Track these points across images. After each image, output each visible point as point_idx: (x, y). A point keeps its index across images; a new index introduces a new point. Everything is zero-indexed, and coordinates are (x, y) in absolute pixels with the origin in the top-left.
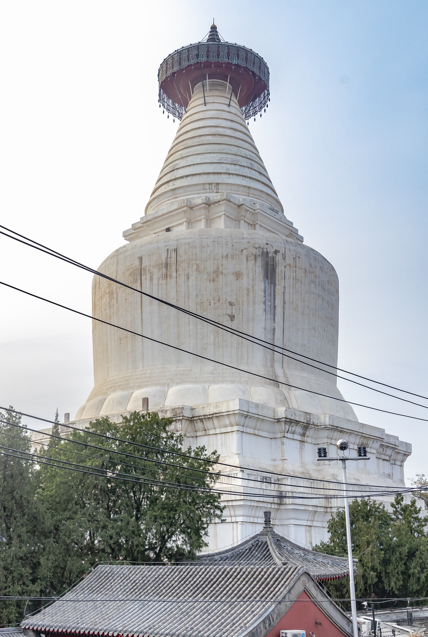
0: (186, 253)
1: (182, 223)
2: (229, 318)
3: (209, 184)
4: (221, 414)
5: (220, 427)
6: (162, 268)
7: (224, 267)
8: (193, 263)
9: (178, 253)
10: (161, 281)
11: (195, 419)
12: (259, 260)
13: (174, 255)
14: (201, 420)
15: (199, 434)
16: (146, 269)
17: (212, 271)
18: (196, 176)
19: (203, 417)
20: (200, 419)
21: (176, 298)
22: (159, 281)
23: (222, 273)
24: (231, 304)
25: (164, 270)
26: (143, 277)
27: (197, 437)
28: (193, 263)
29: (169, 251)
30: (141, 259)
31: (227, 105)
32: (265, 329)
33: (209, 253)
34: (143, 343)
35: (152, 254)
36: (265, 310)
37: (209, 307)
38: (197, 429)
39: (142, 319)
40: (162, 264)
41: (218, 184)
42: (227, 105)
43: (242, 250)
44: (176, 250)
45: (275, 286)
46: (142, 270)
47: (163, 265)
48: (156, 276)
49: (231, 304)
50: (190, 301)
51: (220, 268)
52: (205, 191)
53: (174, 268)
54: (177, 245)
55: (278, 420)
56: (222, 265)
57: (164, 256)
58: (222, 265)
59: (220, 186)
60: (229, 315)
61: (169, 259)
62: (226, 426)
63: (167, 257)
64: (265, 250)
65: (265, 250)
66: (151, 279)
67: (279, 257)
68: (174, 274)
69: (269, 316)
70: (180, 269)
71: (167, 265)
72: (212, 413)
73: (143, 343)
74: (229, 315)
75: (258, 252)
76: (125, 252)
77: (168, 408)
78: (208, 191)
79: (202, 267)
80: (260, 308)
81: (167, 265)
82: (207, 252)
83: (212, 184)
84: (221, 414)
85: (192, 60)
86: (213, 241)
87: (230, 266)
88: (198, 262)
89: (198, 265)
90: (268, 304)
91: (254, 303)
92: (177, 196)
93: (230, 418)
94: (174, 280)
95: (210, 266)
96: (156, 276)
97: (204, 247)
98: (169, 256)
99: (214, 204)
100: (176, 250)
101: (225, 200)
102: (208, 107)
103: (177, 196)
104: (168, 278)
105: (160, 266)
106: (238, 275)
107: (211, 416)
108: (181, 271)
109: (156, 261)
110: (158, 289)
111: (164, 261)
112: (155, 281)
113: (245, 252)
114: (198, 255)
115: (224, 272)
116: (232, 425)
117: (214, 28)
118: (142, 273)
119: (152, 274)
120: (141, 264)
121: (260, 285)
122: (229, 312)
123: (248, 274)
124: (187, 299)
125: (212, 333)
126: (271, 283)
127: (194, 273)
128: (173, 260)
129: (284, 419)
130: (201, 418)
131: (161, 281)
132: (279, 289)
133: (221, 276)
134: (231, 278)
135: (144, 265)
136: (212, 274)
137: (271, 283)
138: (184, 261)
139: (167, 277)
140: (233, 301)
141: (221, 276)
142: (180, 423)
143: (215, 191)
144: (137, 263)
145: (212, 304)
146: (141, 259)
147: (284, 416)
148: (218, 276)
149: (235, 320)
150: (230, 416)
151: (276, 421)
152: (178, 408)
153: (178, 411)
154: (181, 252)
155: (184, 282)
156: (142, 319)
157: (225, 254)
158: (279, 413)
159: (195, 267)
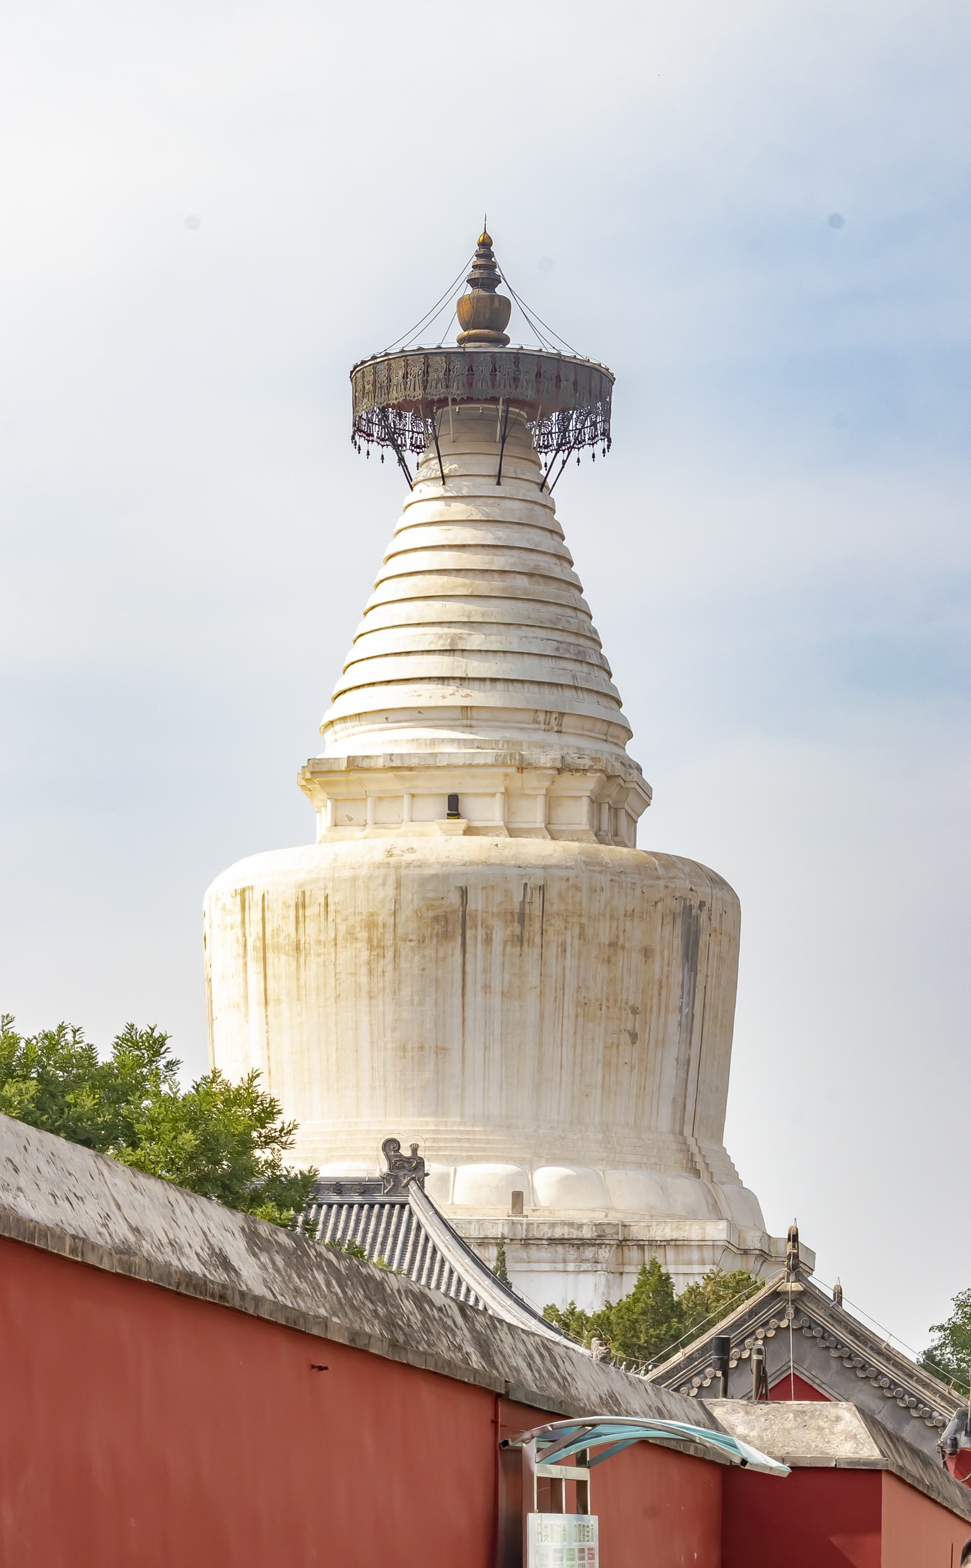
0: (560, 896)
2: (628, 1038)
3: (546, 712)
4: (686, 1243)
6: (513, 921)
8: (574, 920)
10: (509, 949)
11: (628, 1243)
12: (679, 922)
13: (537, 899)
14: (641, 1247)
16: (476, 916)
17: (607, 943)
18: (515, 684)
19: (647, 1243)
21: (538, 989)
22: (504, 947)
23: (623, 947)
24: (634, 1011)
25: (517, 927)
26: (469, 934)
27: (621, 1274)
28: (574, 920)
29: (529, 889)
30: (464, 892)
31: (537, 484)
32: (677, 1060)
33: (602, 903)
34: (463, 1067)
36: (680, 1025)
37: (598, 1013)
39: (464, 1019)
40: (512, 913)
42: (537, 484)
43: (656, 903)
44: (542, 889)
45: (696, 974)
46: (468, 918)
47: (516, 917)
48: (499, 935)
50: (566, 997)
52: (536, 726)
53: (537, 925)
54: (545, 879)
55: (746, 1252)
57: (518, 897)
59: (566, 719)
60: (629, 1033)
61: (527, 906)
62: (690, 1263)
63: (523, 902)
64: (688, 903)
65: (688, 903)
66: (488, 940)
67: (704, 917)
68: (538, 939)
69: (684, 1036)
71: (522, 918)
72: (668, 1238)
73: (463, 1067)
75: (678, 907)
76: (420, 866)
77: (585, 1221)
78: (543, 727)
79: (589, 932)
80: (674, 1019)
81: (522, 918)
82: (599, 901)
83: (551, 712)
84: (686, 1243)
86: (612, 880)
87: (636, 934)
88: (584, 920)
89: (582, 926)
90: (685, 1010)
92: (473, 723)
93: (702, 1252)
94: (537, 951)
95: (604, 932)
96: (499, 935)
97: (596, 891)
98: (528, 900)
100: (542, 889)
101: (601, 771)
102: (507, 488)
104: (526, 944)
105: (509, 917)
106: (647, 953)
107: (663, 1243)
108: (551, 934)
109: (501, 903)
110: (503, 963)
112: (497, 946)
113: (660, 905)
114: (584, 904)
115: (627, 945)
117: (486, 244)
119: (492, 930)
120: (464, 903)
121: (677, 974)
124: (559, 994)
125: (600, 1065)
127: (576, 941)
128: (537, 911)
129: (758, 1252)
130: (642, 1243)
131: (509, 949)
133: (620, 952)
134: (636, 957)
135: (471, 906)
136: (607, 947)
138: (558, 914)
139: (522, 941)
141: (620, 952)
142: (607, 1250)
143: (556, 729)
144: (455, 898)
146: (464, 892)
147: (758, 1246)
148: (615, 953)
149: (638, 1042)
150: (705, 1248)
151: (739, 1252)
152: (609, 1224)
154: (552, 892)
155: (557, 958)
156: (464, 1019)
157: (630, 909)
158: (749, 1239)
159: (577, 930)
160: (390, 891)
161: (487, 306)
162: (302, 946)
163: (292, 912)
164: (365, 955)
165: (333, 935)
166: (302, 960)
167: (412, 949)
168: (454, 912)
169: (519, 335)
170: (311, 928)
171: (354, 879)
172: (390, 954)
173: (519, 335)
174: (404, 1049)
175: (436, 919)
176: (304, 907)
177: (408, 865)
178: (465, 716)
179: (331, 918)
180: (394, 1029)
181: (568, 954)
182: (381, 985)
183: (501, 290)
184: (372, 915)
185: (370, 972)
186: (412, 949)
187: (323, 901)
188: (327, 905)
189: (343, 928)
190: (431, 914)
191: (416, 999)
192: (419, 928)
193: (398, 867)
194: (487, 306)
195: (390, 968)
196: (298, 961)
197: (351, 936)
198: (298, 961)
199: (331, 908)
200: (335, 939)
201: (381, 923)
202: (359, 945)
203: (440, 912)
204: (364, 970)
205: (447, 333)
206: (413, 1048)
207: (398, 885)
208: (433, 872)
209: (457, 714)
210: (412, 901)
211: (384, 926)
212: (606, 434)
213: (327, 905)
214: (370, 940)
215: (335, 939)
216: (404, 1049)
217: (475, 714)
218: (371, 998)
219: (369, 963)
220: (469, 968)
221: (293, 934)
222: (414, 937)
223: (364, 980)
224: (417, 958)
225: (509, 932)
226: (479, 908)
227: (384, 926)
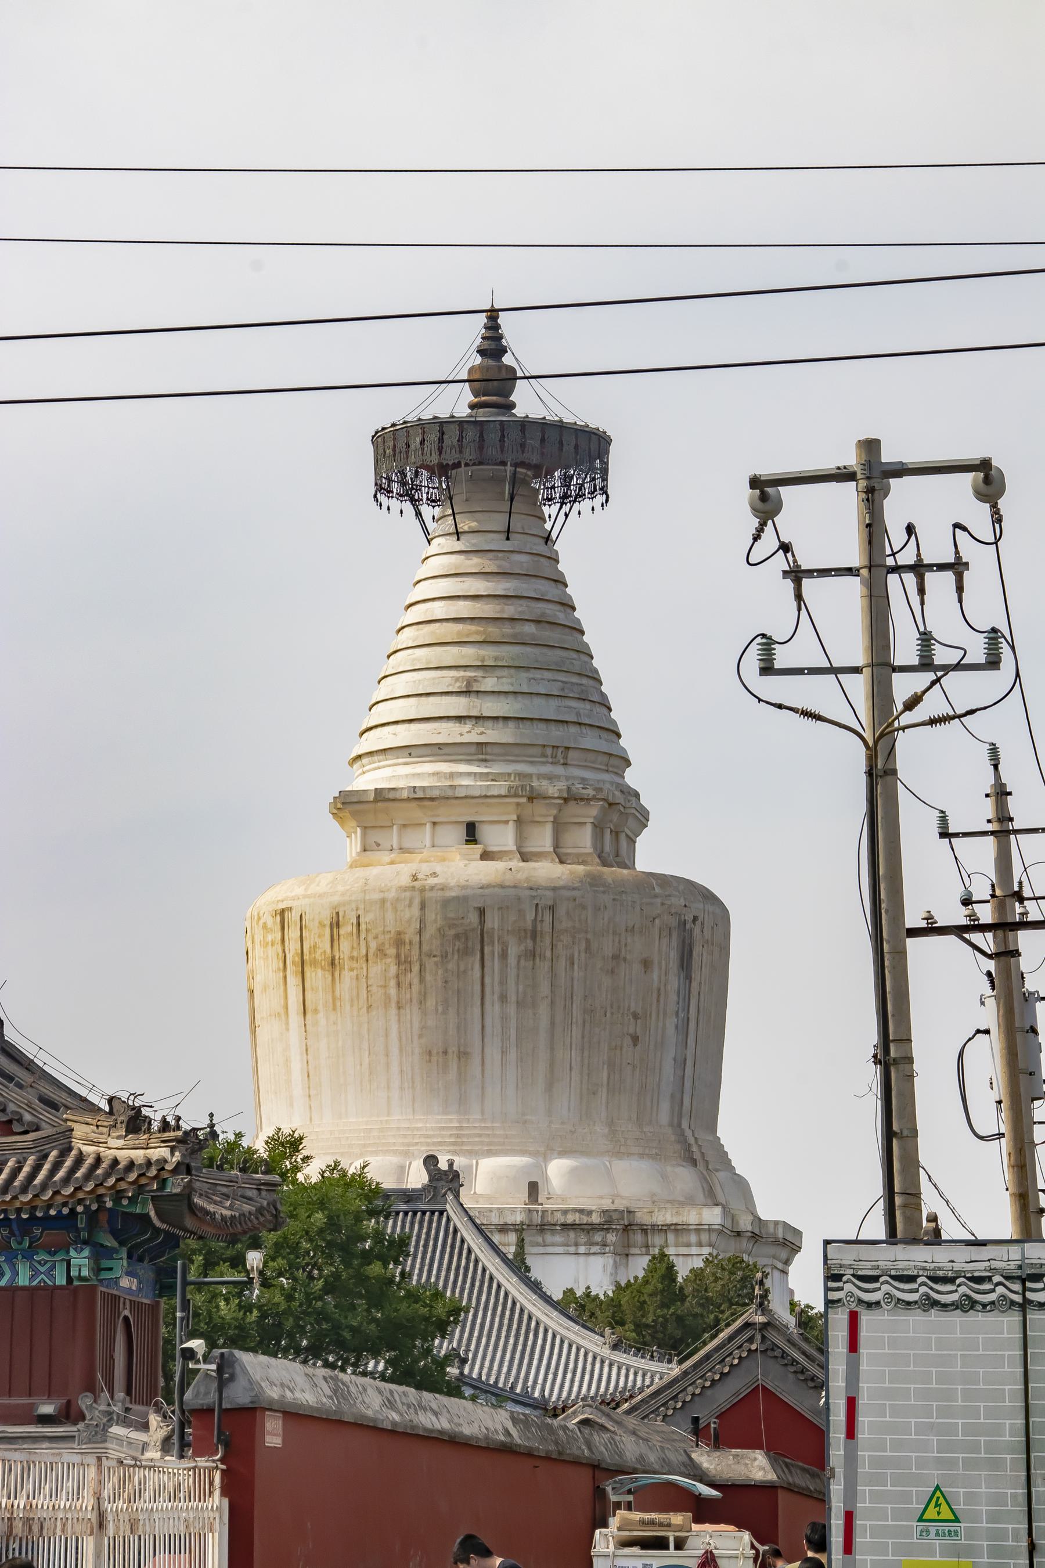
1: (507, 822)
5: (676, 1246)
6: (526, 937)
7: (629, 948)
9: (556, 916)
13: (548, 918)
14: (645, 1231)
15: (633, 1251)
20: (642, 1230)
23: (625, 959)
24: (636, 1016)
25: (530, 943)
27: (627, 1255)
30: (482, 912)
33: (606, 919)
35: (508, 907)
38: (632, 1242)
40: (525, 931)
41: (568, 748)
44: (552, 908)
46: (485, 935)
47: (529, 934)
49: (636, 1016)
51: (623, 950)
53: (548, 941)
54: (554, 900)
55: (739, 1234)
56: (626, 945)
57: (530, 916)
58: (626, 945)
59: (571, 754)
60: (631, 1035)
62: (689, 1245)
66: (504, 955)
68: (548, 954)
70: (560, 945)
74: (631, 1035)
76: (442, 889)
78: (550, 760)
81: (534, 935)
83: (558, 747)
85: (510, 452)
88: (589, 936)
89: (588, 941)
90: (681, 1015)
91: (665, 1014)
92: (488, 757)
96: (513, 951)
98: (539, 918)
99: (576, 799)
100: (552, 908)
101: (603, 799)
103: (488, 757)
105: (523, 934)
106: (646, 964)
110: (518, 976)
111: (529, 925)
113: (657, 921)
116: (700, 1244)
118: (486, 939)
122: (631, 1030)
123: (660, 963)
126: (687, 978)
127: (583, 955)
128: (547, 927)
132: (695, 985)
134: (637, 968)
135: (488, 925)
137: (687, 978)
139: (534, 956)
140: (639, 1011)
143: (562, 761)
144: (473, 918)
145: (608, 1015)
146: (482, 912)
147: (750, 1228)
149: (639, 1045)
153: (615, 1216)
154: (561, 911)
160: (416, 911)
161: (494, 378)
162: (337, 962)
163: (328, 931)
164: (393, 969)
165: (364, 952)
166: (337, 974)
167: (436, 964)
168: (473, 930)
169: (526, 402)
170: (345, 946)
171: (383, 901)
172: (416, 968)
173: (526, 402)
174: (430, 1053)
175: (457, 936)
176: (338, 926)
177: (432, 888)
178: (480, 751)
179: (362, 936)
180: (420, 1036)
181: (576, 967)
182: (408, 996)
183: (507, 360)
184: (399, 933)
185: (399, 985)
186: (436, 964)
187: (355, 922)
188: (359, 924)
189: (373, 945)
190: (452, 932)
191: (440, 1009)
192: (442, 945)
193: (422, 890)
194: (494, 378)
195: (416, 981)
196: (333, 975)
197: (381, 952)
198: (333, 975)
199: (363, 927)
200: (367, 955)
201: (407, 941)
202: (389, 960)
203: (460, 930)
204: (393, 983)
205: (457, 403)
206: (438, 1053)
207: (423, 906)
208: (453, 894)
209: (473, 749)
210: (435, 921)
211: (411, 943)
212: (604, 491)
213: (359, 924)
214: (398, 956)
215: (367, 955)
216: (430, 1053)
217: (489, 749)
218: (399, 1008)
219: (397, 976)
220: (487, 980)
221: (329, 951)
222: (438, 953)
223: (393, 991)
224: (440, 972)
225: (522, 947)
226: (496, 927)
227: (411, 943)
